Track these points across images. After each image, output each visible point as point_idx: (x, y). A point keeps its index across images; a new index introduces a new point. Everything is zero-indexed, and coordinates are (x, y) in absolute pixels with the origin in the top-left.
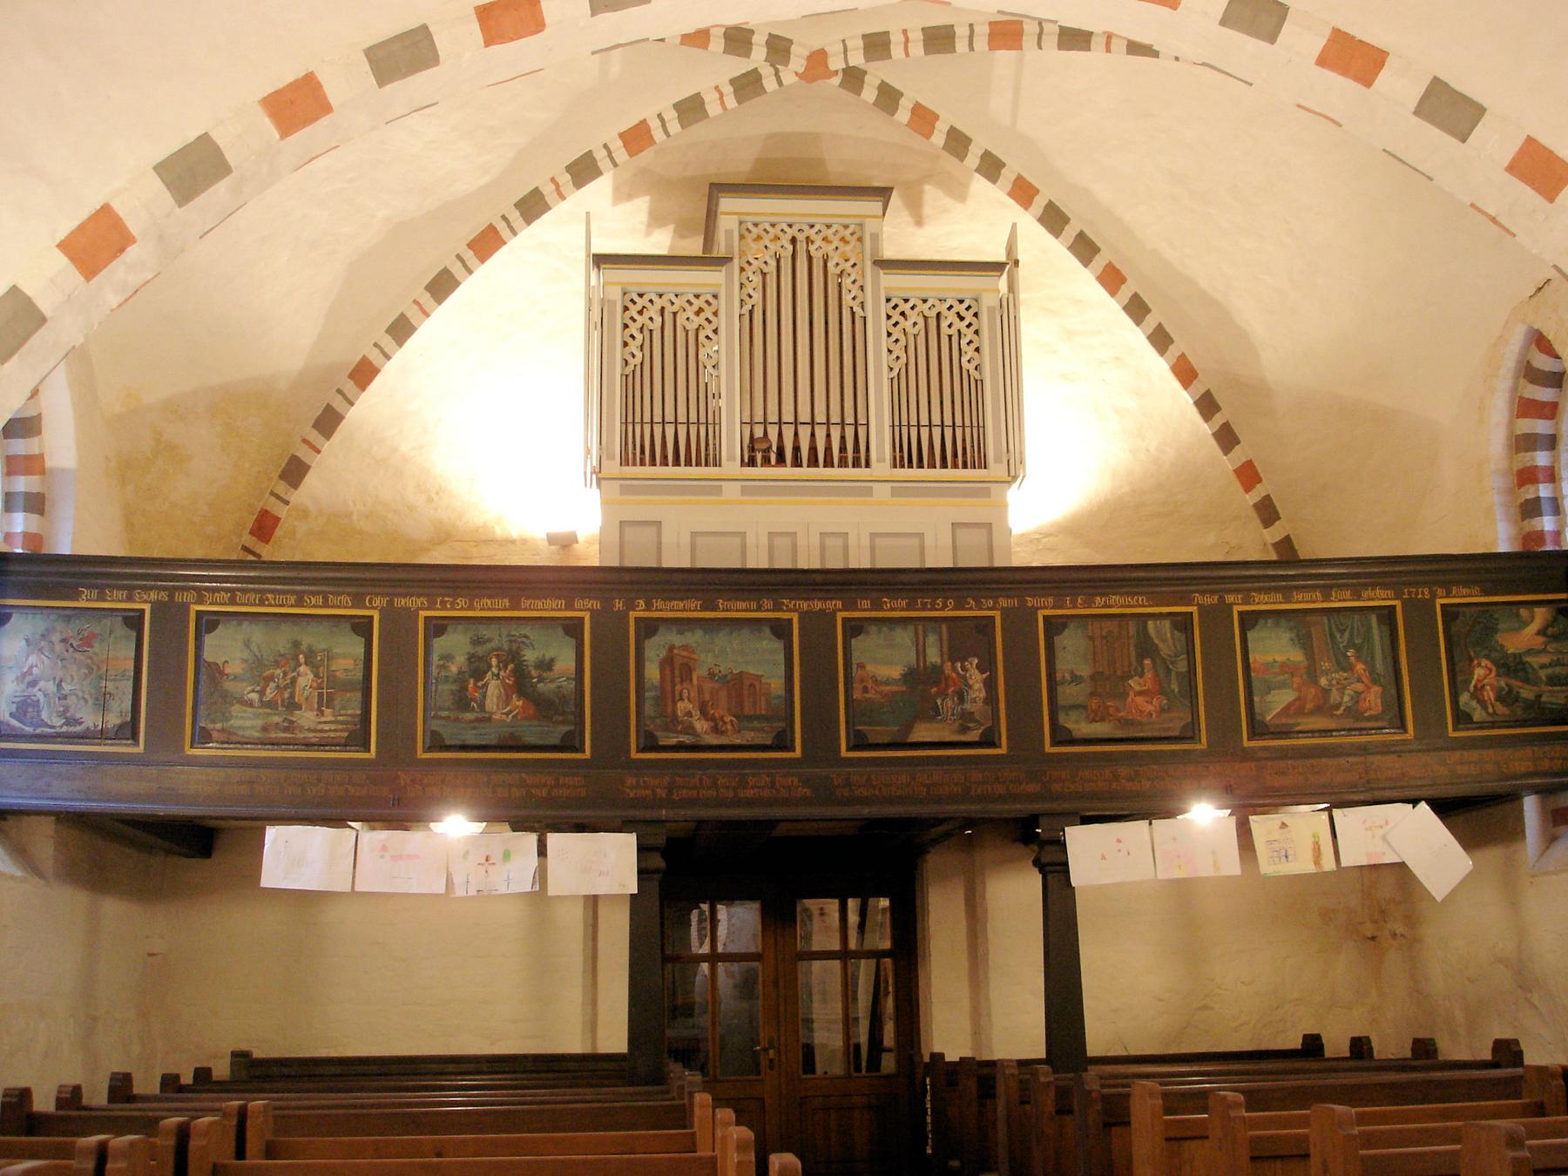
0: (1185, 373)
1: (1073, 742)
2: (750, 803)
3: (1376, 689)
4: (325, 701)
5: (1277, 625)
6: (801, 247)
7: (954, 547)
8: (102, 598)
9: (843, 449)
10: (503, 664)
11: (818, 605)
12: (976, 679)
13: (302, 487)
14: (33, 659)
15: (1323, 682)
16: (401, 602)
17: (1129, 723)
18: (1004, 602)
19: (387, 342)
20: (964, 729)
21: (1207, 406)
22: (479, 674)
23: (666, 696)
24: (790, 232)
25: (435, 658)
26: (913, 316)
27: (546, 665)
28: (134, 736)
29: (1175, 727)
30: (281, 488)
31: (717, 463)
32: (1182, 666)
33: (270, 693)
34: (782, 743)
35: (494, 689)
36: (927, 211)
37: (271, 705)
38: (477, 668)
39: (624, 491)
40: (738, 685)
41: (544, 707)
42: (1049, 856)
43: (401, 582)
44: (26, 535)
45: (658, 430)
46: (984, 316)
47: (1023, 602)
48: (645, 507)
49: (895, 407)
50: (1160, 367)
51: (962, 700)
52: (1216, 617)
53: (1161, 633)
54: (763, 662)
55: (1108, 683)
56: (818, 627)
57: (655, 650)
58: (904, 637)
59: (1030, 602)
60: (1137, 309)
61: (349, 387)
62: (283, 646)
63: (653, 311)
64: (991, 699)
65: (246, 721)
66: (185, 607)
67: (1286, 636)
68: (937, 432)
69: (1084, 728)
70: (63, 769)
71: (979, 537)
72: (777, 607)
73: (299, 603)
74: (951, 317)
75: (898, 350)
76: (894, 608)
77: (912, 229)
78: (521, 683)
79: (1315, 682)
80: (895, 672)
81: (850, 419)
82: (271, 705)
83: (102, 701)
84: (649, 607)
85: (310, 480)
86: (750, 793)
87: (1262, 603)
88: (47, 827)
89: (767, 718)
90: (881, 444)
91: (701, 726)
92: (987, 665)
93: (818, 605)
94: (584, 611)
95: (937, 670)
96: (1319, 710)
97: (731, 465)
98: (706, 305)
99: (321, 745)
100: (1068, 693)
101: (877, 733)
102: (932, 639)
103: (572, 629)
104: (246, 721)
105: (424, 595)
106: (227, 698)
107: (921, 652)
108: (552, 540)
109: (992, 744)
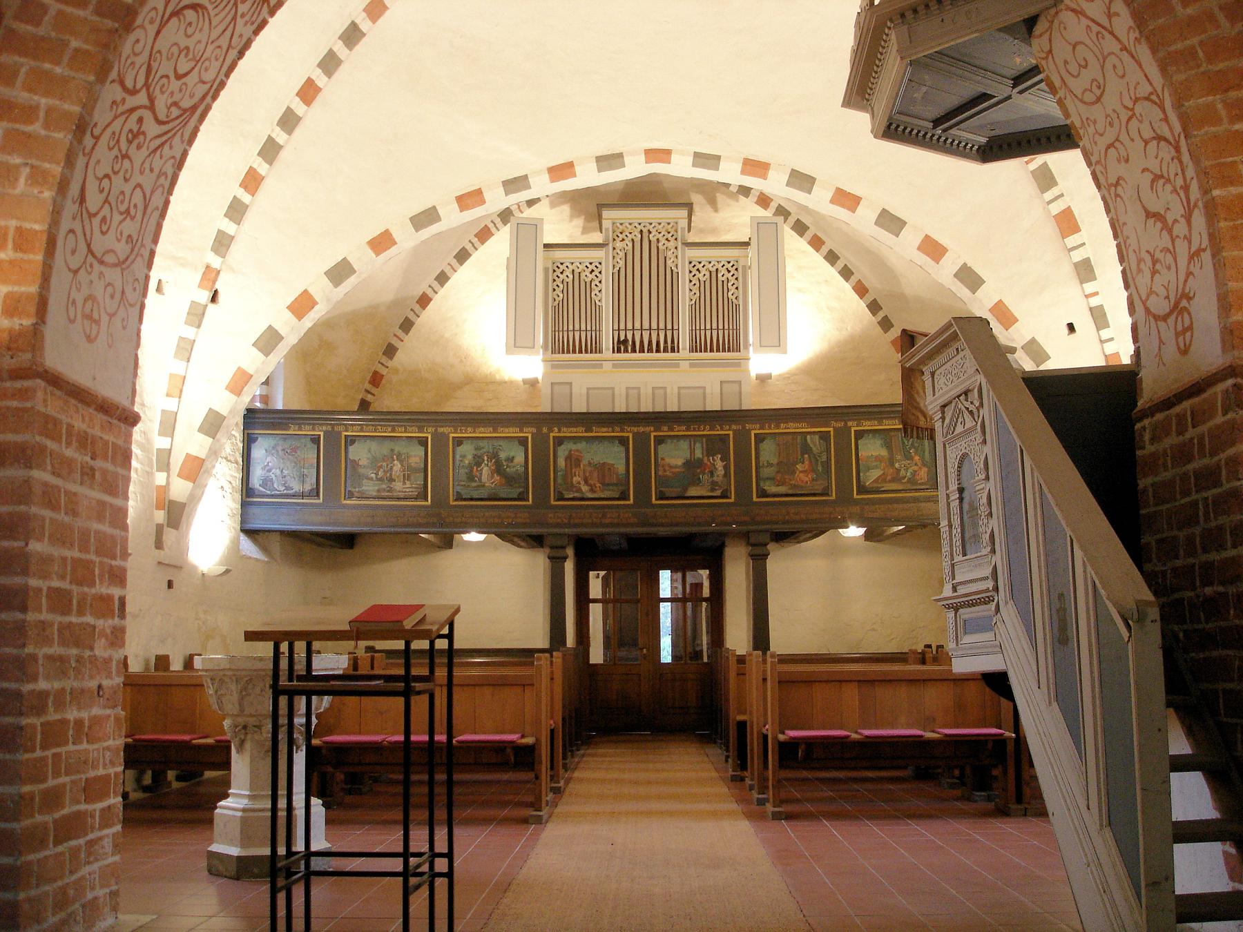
0: (861, 290)
1: (768, 496)
2: (607, 526)
3: (925, 470)
4: (406, 478)
5: (874, 437)
6: (645, 234)
7: (170, 685)
8: (300, 429)
9: (666, 342)
10: (490, 459)
11: (642, 429)
12: (719, 465)
13: (395, 359)
14: (269, 459)
15: (897, 465)
16: (441, 430)
17: (795, 486)
18: (734, 427)
19: (436, 285)
20: (713, 490)
21: (874, 307)
22: (478, 464)
23: (568, 475)
24: (639, 228)
25: (458, 457)
26: (703, 271)
27: (511, 459)
28: (318, 495)
29: (819, 487)
30: (384, 360)
31: (601, 352)
32: (824, 458)
33: (381, 474)
34: (624, 496)
35: (486, 471)
36: (719, 206)
37: (381, 480)
38: (478, 461)
39: (553, 367)
40: (603, 469)
41: (510, 480)
42: (758, 551)
43: (440, 421)
44: (261, 396)
45: (571, 334)
46: (740, 270)
47: (744, 427)
48: (563, 376)
49: (693, 320)
50: (847, 287)
51: (712, 475)
52: (843, 434)
53: (814, 443)
54: (615, 458)
55: (785, 467)
56: (642, 441)
57: (562, 452)
58: (684, 445)
59: (748, 426)
60: (832, 258)
61: (417, 308)
62: (385, 451)
63: (568, 272)
64: (727, 475)
65: (370, 488)
66: (340, 433)
67: (879, 442)
68: (715, 333)
69: (773, 489)
70: (285, 511)
71: (735, 387)
72: (622, 431)
73: (393, 431)
74: (723, 271)
75: (695, 289)
76: (680, 430)
77: (714, 214)
78: (498, 469)
79: (892, 464)
80: (680, 462)
81: (669, 327)
82: (381, 480)
83: (303, 478)
84: (559, 431)
85: (399, 355)
86: (607, 521)
87: (867, 425)
88: (277, 537)
89: (616, 485)
90: (684, 340)
91: (585, 488)
92: (725, 458)
93: (642, 429)
94: (528, 433)
95: (700, 461)
96: (893, 480)
97: (607, 353)
98: (595, 268)
99: (405, 499)
100: (766, 472)
101: (669, 492)
102: (698, 445)
103: (523, 442)
104: (370, 488)
105: (453, 423)
106: (361, 477)
107: (692, 452)
108: (525, 382)
109: (727, 497)
